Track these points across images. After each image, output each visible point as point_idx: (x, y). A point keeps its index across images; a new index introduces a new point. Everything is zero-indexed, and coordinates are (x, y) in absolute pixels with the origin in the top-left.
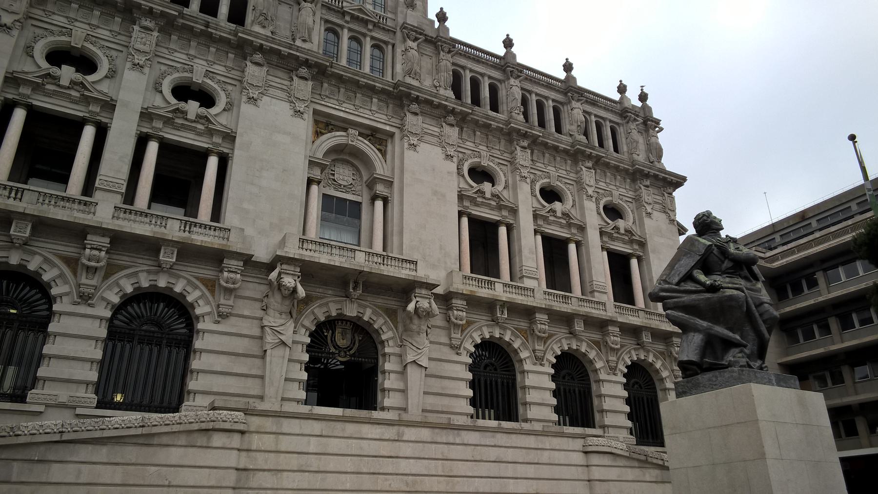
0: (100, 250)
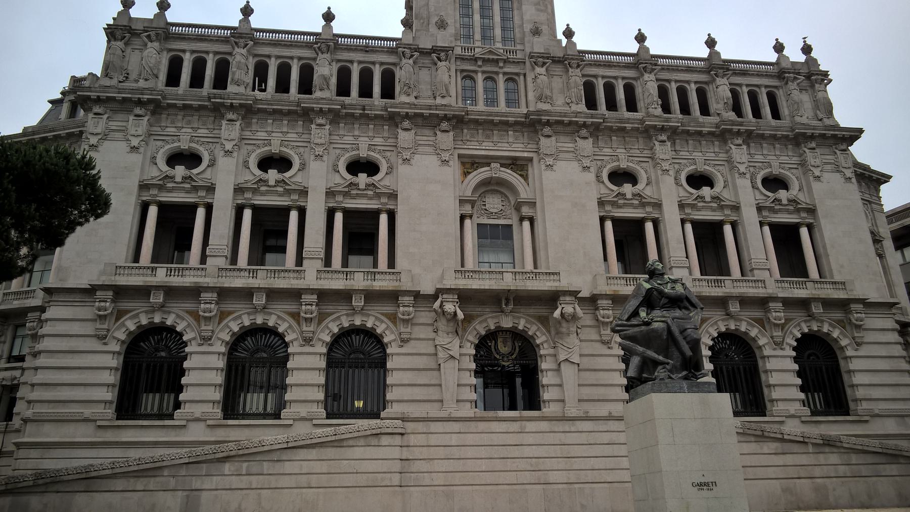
0: (312, 305)
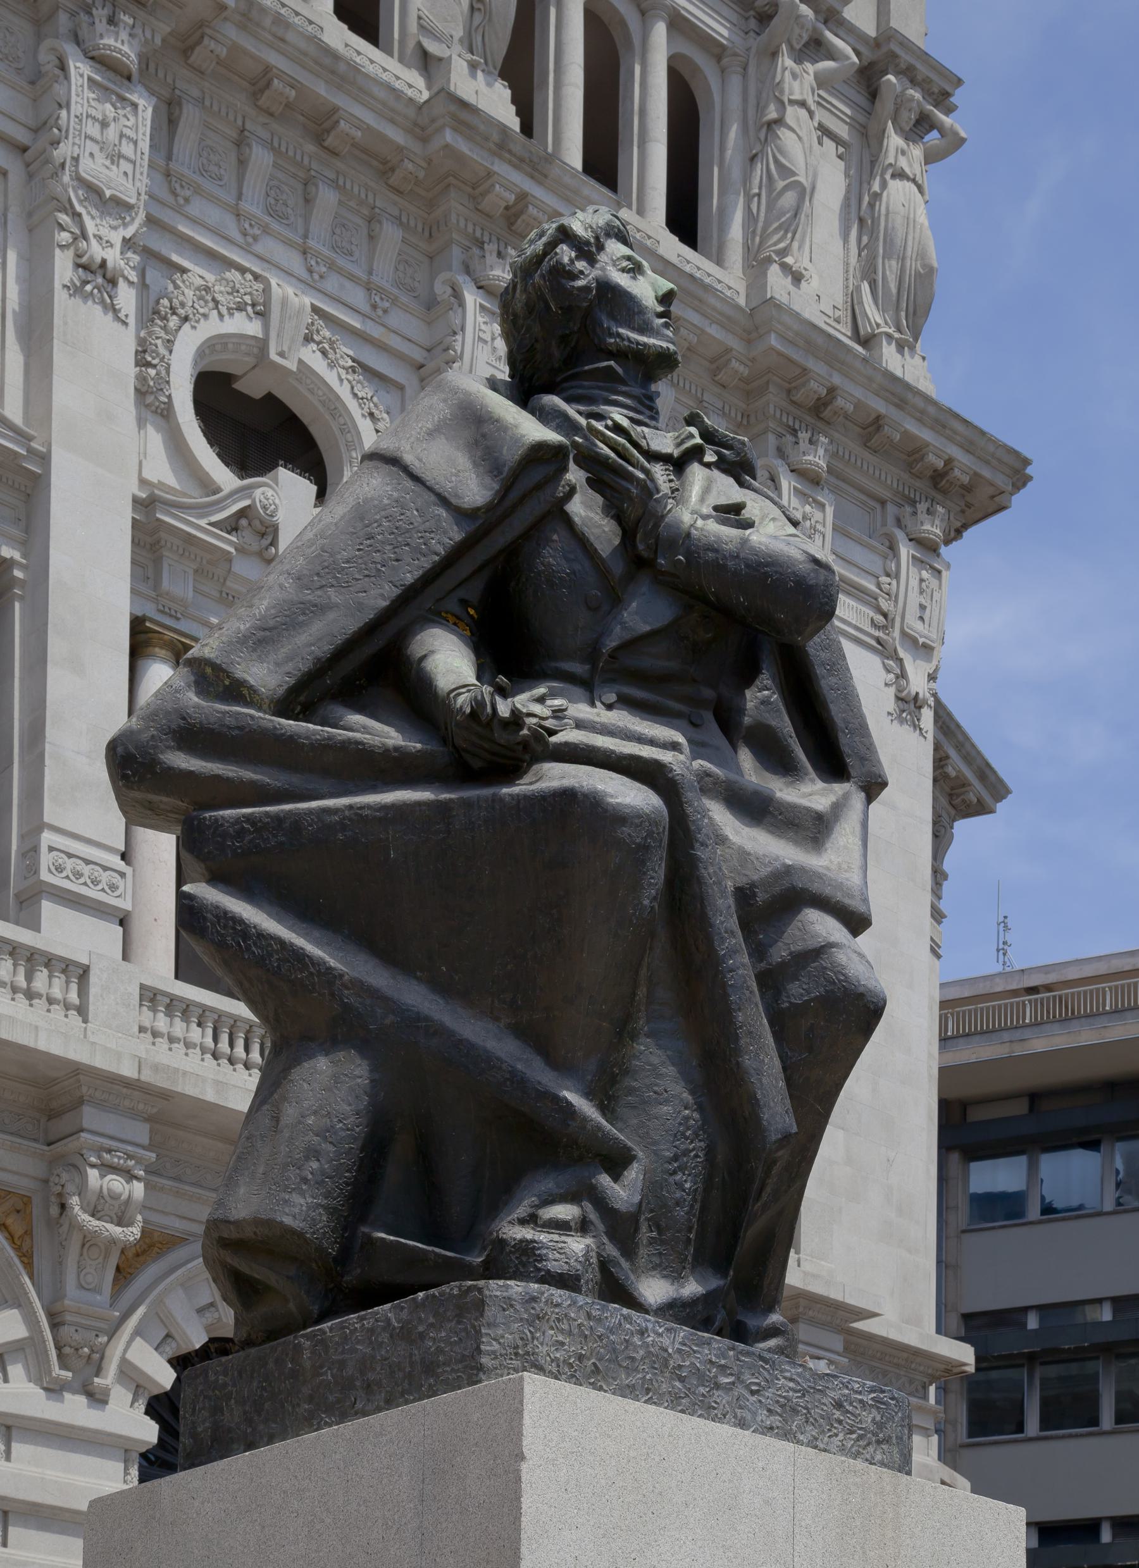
0: (130, 1176)
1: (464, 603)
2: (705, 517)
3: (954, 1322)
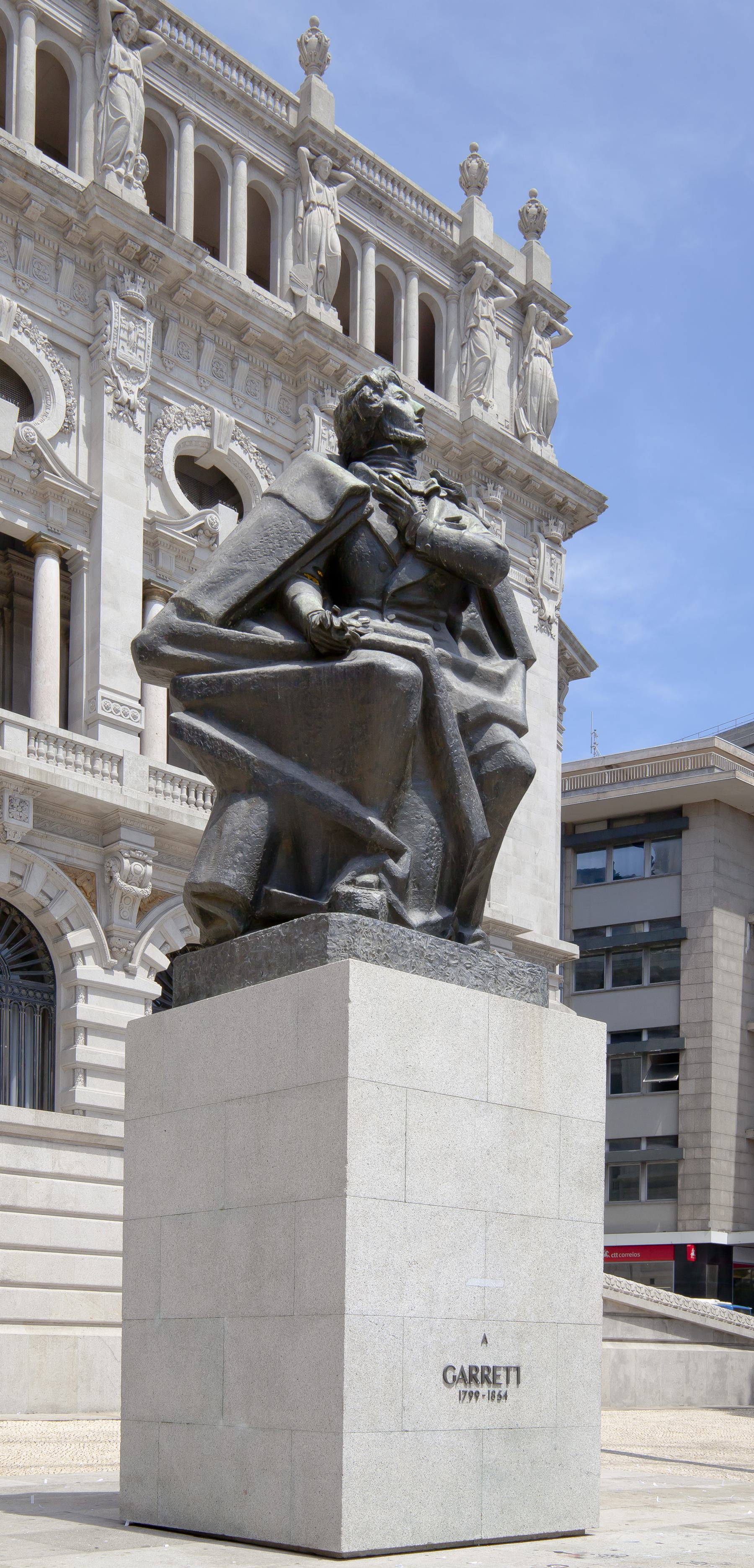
0: (146, 863)
1: (316, 569)
2: (441, 524)
3: (569, 934)
